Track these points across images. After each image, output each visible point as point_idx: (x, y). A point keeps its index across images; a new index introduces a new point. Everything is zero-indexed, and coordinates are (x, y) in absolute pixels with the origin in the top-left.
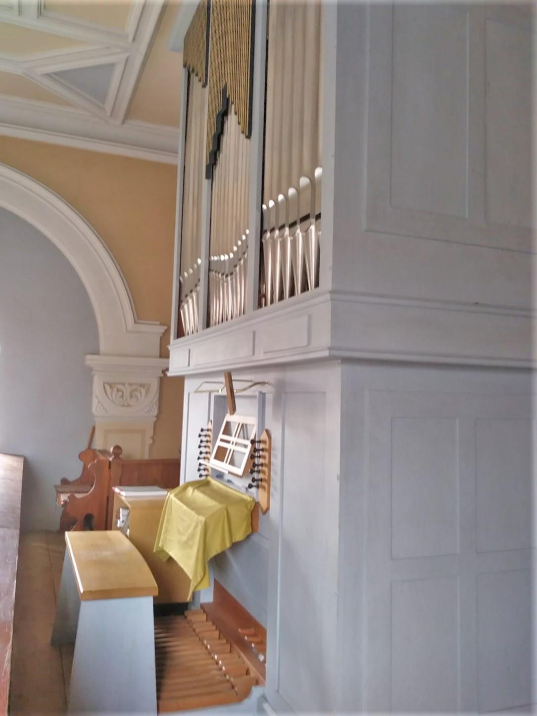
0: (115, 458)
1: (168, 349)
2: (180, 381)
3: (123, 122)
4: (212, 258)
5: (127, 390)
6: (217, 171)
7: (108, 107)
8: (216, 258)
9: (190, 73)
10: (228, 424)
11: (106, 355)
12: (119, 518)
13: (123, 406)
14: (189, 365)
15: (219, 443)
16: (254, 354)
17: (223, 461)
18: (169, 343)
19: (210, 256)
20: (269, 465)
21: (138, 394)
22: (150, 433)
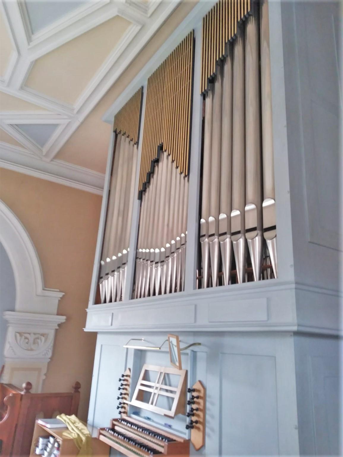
0: (26, 393)
1: (86, 311)
2: (93, 336)
3: (52, 160)
4: (140, 250)
5: (31, 338)
6: (146, 197)
7: (45, 150)
9: (116, 134)
10: (146, 372)
11: (19, 312)
12: (37, 446)
13: (28, 350)
14: (112, 325)
15: (139, 387)
16: (195, 321)
17: (148, 402)
18: (87, 308)
19: (137, 248)
20: (204, 410)
21: (39, 341)
22: (44, 371)
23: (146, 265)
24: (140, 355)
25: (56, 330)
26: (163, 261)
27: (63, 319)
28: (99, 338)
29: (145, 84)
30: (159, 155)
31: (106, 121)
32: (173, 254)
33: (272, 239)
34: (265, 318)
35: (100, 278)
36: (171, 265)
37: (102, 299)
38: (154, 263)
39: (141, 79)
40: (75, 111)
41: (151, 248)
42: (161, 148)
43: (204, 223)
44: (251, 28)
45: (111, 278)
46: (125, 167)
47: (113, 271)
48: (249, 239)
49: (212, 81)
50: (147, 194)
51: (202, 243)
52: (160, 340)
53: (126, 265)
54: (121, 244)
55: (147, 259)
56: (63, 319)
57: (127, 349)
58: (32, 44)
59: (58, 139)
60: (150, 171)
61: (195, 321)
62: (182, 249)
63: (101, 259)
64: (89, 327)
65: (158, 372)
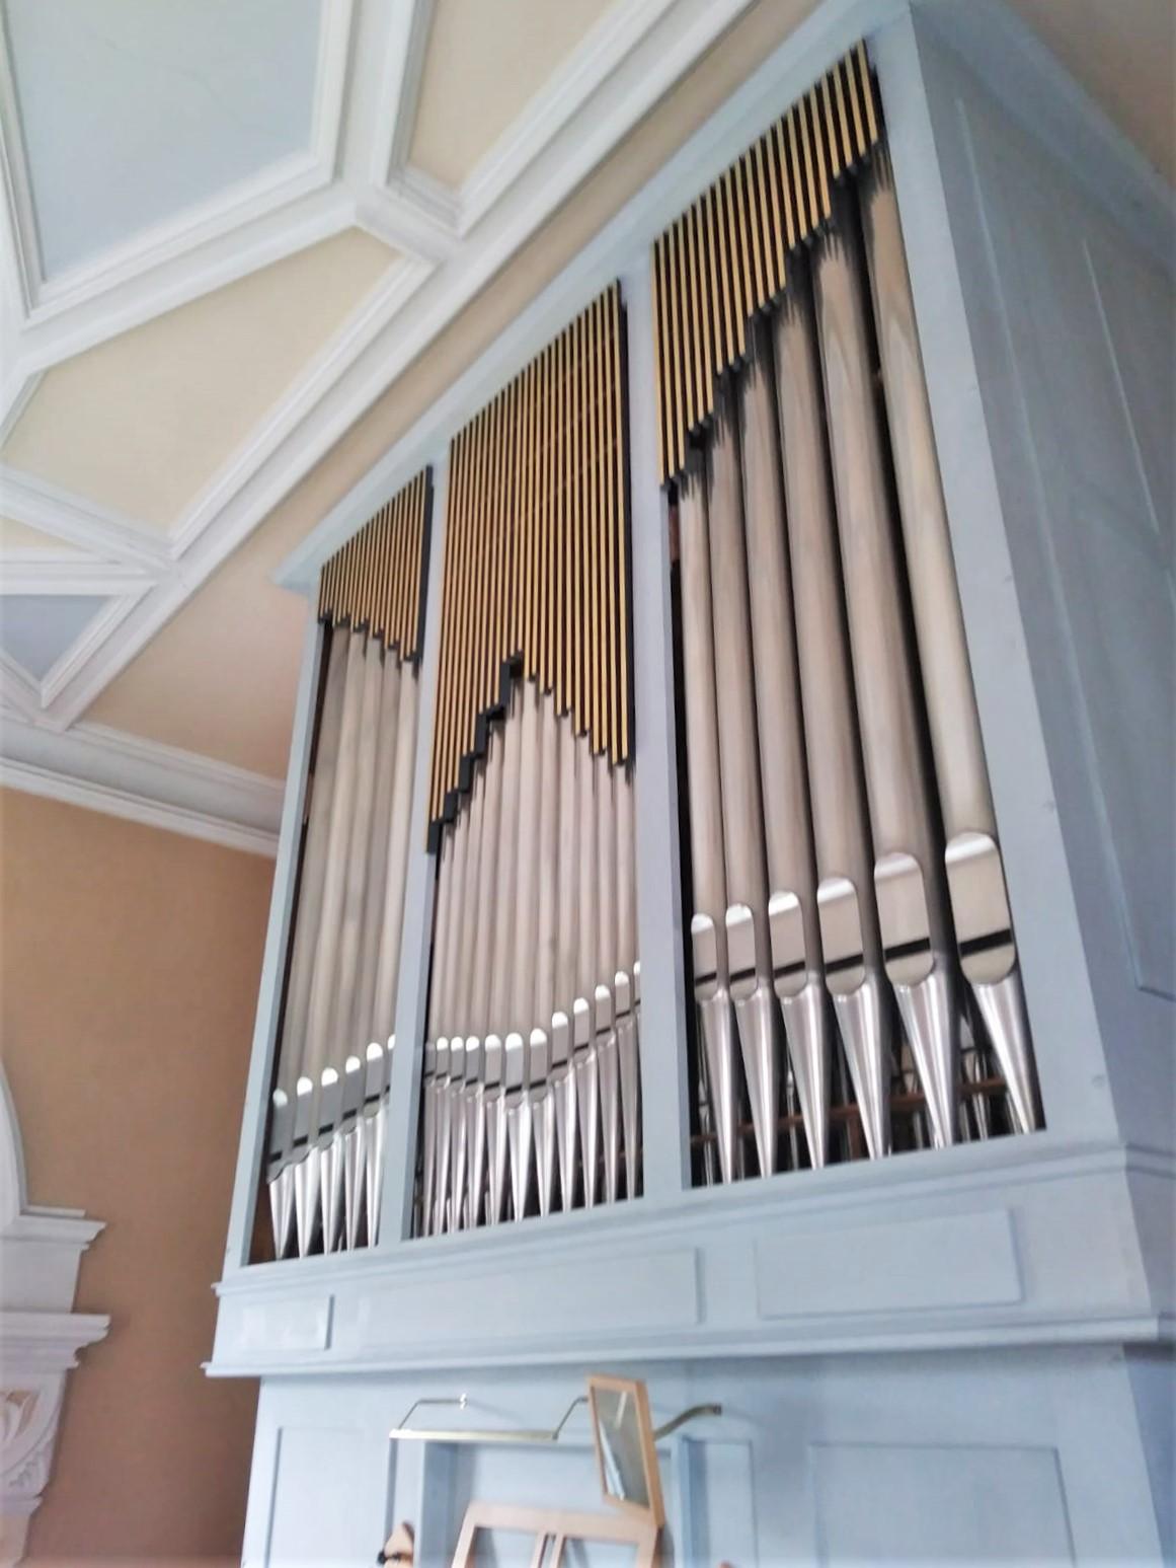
1: (214, 1291)
2: (244, 1393)
3: (71, 727)
4: (442, 1044)
6: (456, 843)
7: (47, 690)
8: (442, 1044)
9: (328, 626)
10: (480, 1535)
14: (328, 1344)
16: (701, 1315)
18: (219, 1279)
23: (469, 1100)
24: (450, 1463)
25: (70, 1375)
26: (541, 1083)
27: (94, 1327)
28: (266, 1394)
29: (441, 459)
30: (506, 695)
31: (289, 586)
32: (583, 1053)
33: (996, 981)
34: (1009, 1290)
35: (269, 1157)
36: (576, 1099)
37: (281, 1238)
38: (503, 1090)
39: (427, 440)
40: (176, 552)
41: (454, 1036)
42: (514, 670)
43: (704, 932)
44: (834, 274)
45: (315, 1157)
46: (368, 746)
47: (327, 1129)
48: (903, 984)
49: (700, 441)
50: (459, 833)
51: (705, 1005)
52: (546, 1403)
53: (382, 1102)
54: (357, 1020)
55: (470, 1075)
56: (94, 1327)
57: (394, 1443)
58: (39, 315)
59: (100, 649)
60: (472, 748)
61: (701, 1315)
62: (620, 1031)
63: (273, 1087)
64: (226, 1360)
65: (535, 1534)
